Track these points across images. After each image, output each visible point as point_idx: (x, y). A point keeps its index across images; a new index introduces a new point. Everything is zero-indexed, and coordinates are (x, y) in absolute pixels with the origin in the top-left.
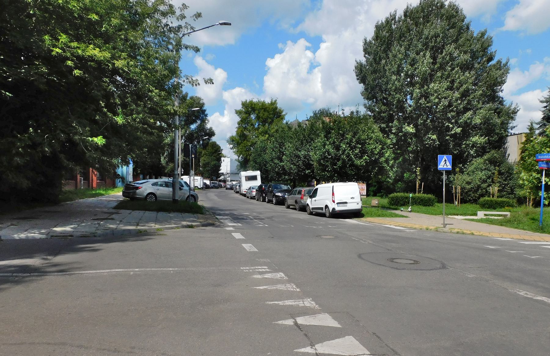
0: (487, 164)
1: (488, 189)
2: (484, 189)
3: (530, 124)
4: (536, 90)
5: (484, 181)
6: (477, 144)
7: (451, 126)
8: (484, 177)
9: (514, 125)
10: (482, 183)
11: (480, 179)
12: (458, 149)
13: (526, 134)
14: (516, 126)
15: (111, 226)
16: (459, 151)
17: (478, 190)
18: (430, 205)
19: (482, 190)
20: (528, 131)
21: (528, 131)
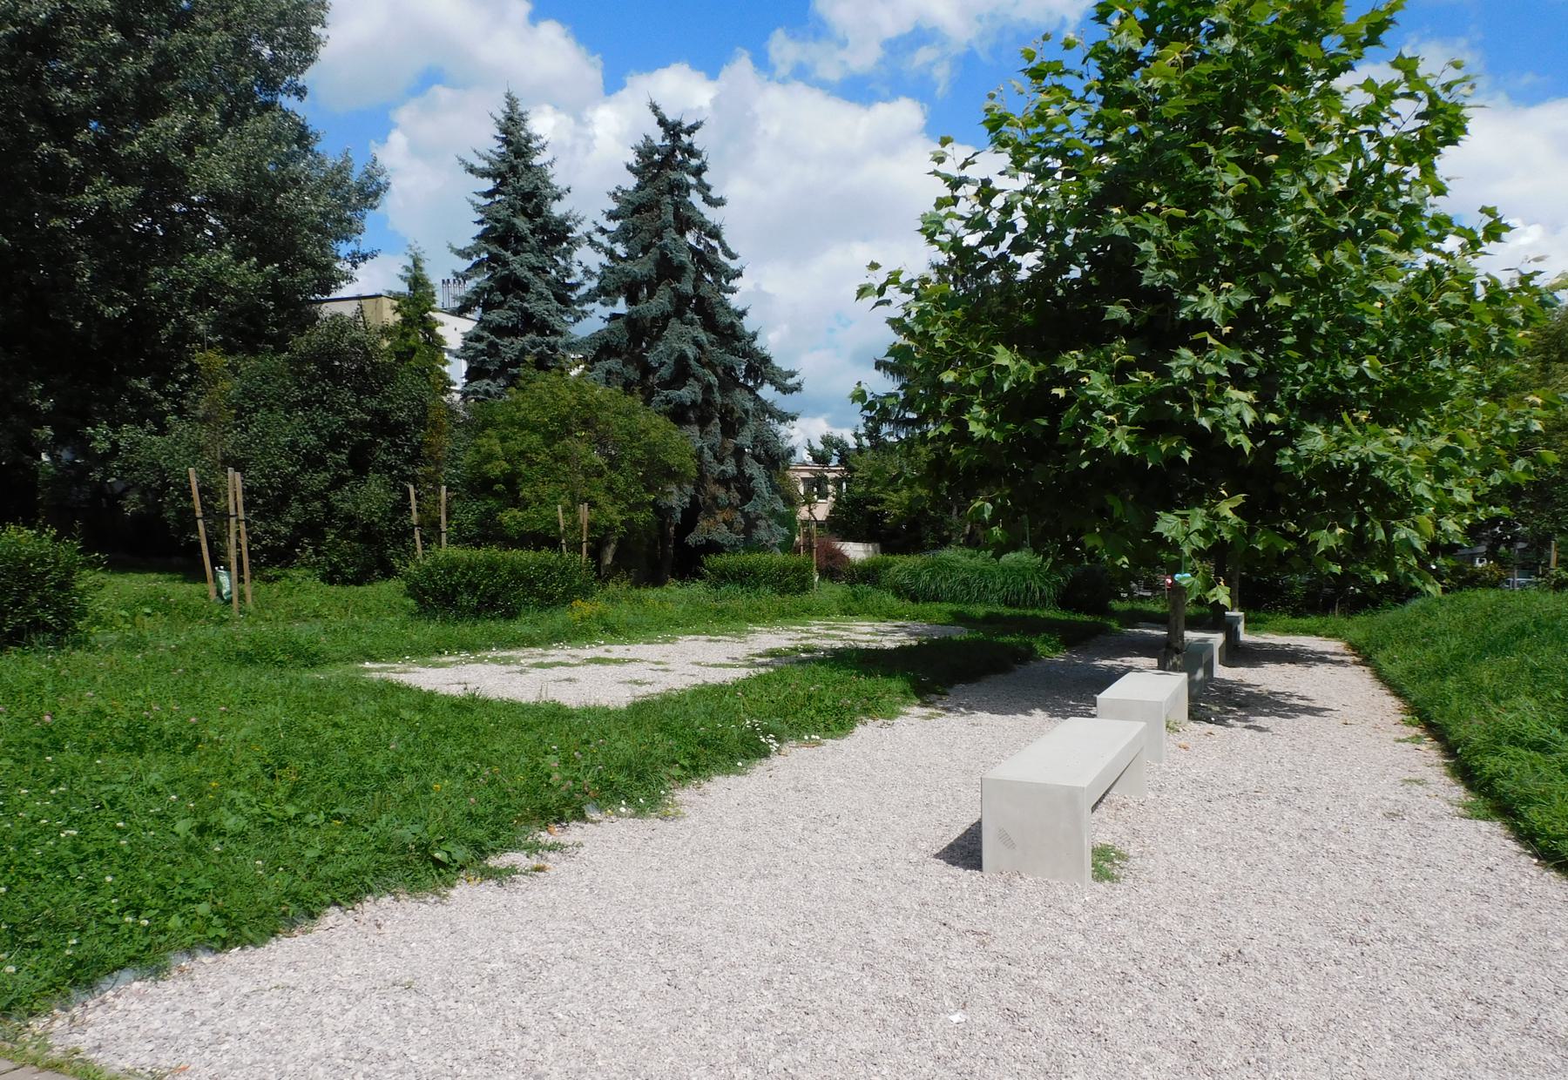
0: (313, 379)
1: (334, 497)
2: (318, 496)
3: (410, 263)
4: (665, 65)
5: (313, 461)
6: (222, 288)
7: (73, 162)
8: (312, 439)
9: (364, 249)
10: (304, 469)
11: (293, 445)
12: (121, 300)
13: (396, 297)
14: (373, 255)
15: (1008, 639)
16: (132, 311)
17: (284, 500)
18: (39, 626)
19: (302, 500)
20: (404, 288)
21: (404, 288)
